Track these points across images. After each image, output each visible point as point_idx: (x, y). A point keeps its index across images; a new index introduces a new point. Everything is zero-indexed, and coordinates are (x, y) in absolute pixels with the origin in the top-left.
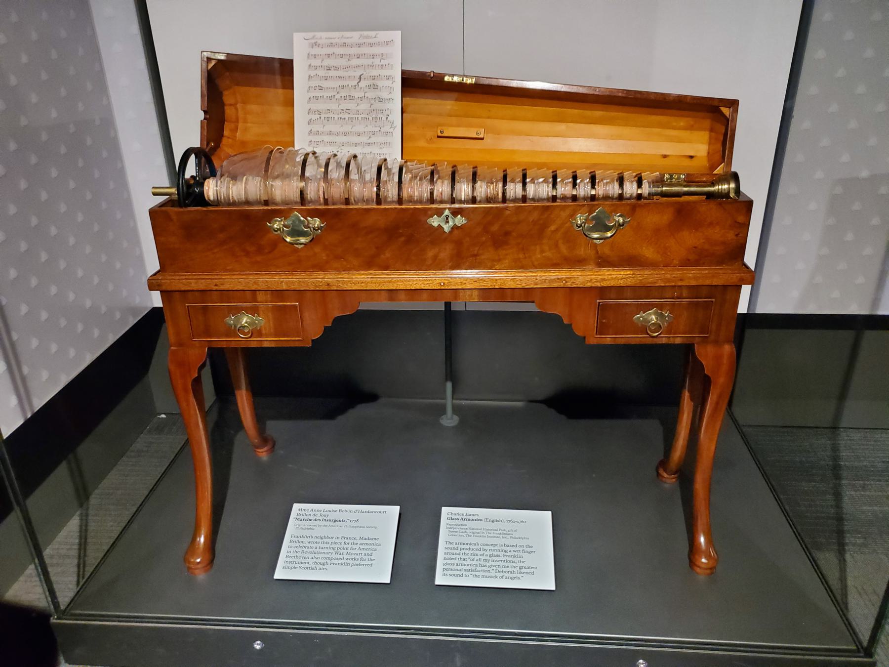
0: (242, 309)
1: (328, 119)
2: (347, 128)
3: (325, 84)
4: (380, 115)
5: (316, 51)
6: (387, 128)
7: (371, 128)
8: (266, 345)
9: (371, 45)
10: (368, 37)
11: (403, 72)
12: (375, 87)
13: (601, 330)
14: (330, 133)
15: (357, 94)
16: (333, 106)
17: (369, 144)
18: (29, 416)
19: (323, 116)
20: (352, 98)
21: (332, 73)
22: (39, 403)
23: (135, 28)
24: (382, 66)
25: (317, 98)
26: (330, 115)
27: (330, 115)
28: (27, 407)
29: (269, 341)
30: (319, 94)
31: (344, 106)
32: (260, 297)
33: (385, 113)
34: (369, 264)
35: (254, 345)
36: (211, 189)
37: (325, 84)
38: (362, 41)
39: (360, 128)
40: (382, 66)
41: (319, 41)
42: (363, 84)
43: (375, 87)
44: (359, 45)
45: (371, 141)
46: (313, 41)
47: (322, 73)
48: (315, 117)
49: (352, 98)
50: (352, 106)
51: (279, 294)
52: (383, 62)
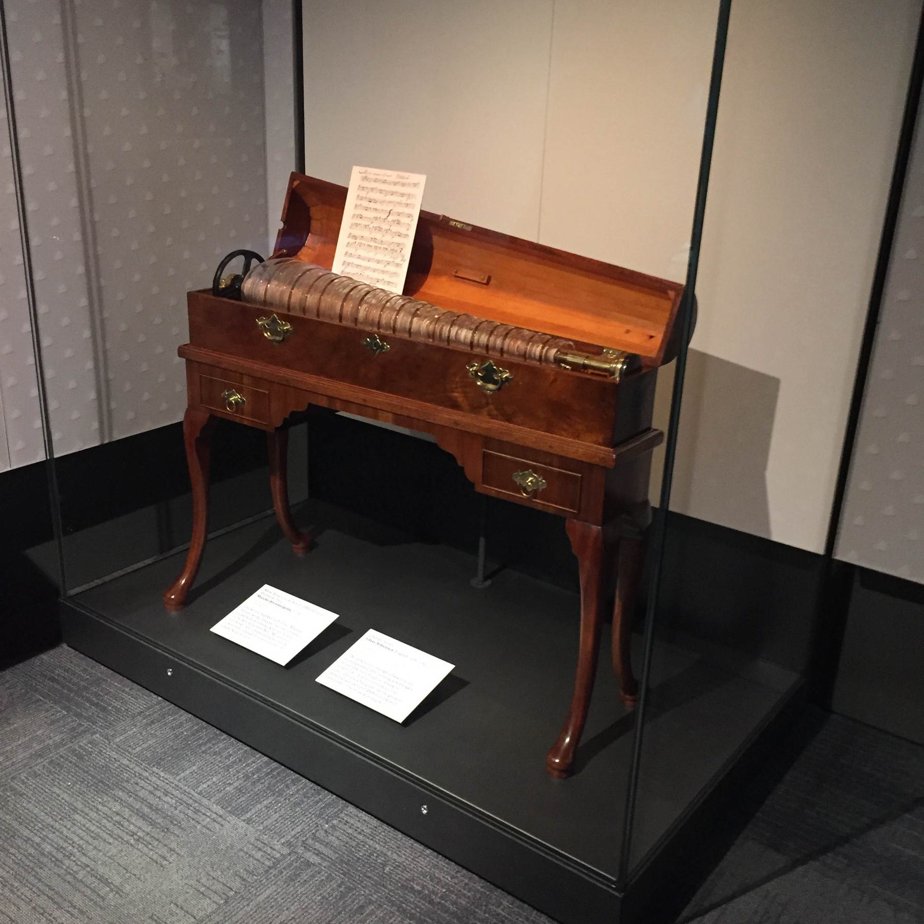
0: (528, 467)
1: (360, 245)
2: (371, 255)
3: (365, 214)
4: (396, 248)
5: (365, 184)
6: (398, 261)
7: (388, 258)
8: (246, 423)
9: (403, 185)
10: (403, 178)
11: (422, 212)
12: (398, 223)
13: (486, 480)
14: (359, 257)
15: (385, 226)
16: (366, 234)
17: (383, 272)
18: (106, 442)
19: (358, 241)
20: (380, 229)
21: (372, 205)
22: (118, 436)
23: (292, 144)
24: (407, 205)
25: (357, 225)
26: (363, 242)
27: (363, 242)
28: (106, 433)
29: (247, 420)
30: (358, 221)
31: (374, 235)
32: (246, 380)
33: (401, 247)
34: (321, 371)
35: (237, 420)
36: (247, 286)
37: (365, 214)
38: (398, 180)
39: (379, 257)
40: (407, 205)
41: (369, 176)
42: (390, 218)
43: (398, 223)
44: (395, 184)
45: (385, 269)
46: (364, 175)
47: (365, 203)
48: (352, 241)
49: (380, 229)
50: (379, 236)
51: (257, 380)
52: (409, 202)
